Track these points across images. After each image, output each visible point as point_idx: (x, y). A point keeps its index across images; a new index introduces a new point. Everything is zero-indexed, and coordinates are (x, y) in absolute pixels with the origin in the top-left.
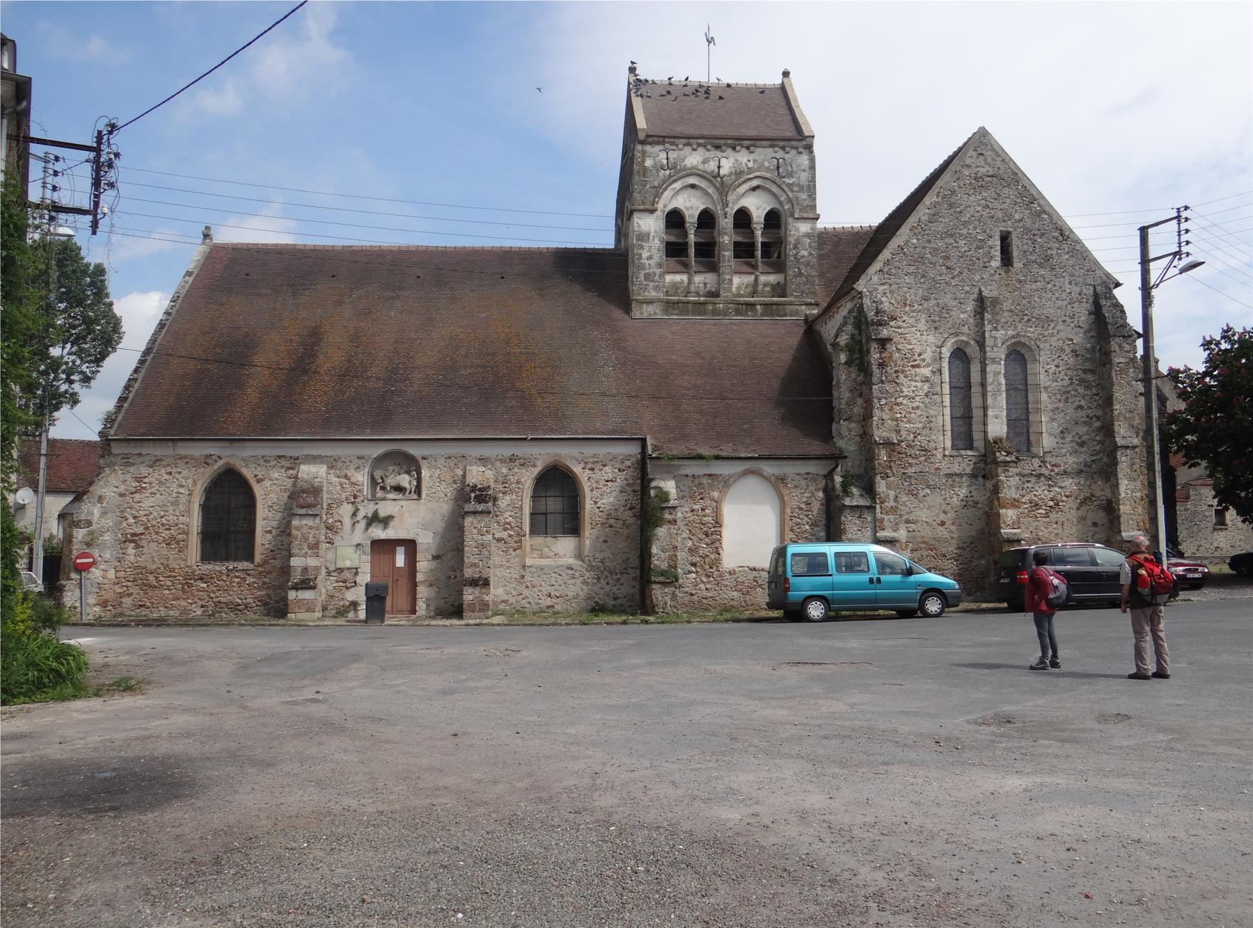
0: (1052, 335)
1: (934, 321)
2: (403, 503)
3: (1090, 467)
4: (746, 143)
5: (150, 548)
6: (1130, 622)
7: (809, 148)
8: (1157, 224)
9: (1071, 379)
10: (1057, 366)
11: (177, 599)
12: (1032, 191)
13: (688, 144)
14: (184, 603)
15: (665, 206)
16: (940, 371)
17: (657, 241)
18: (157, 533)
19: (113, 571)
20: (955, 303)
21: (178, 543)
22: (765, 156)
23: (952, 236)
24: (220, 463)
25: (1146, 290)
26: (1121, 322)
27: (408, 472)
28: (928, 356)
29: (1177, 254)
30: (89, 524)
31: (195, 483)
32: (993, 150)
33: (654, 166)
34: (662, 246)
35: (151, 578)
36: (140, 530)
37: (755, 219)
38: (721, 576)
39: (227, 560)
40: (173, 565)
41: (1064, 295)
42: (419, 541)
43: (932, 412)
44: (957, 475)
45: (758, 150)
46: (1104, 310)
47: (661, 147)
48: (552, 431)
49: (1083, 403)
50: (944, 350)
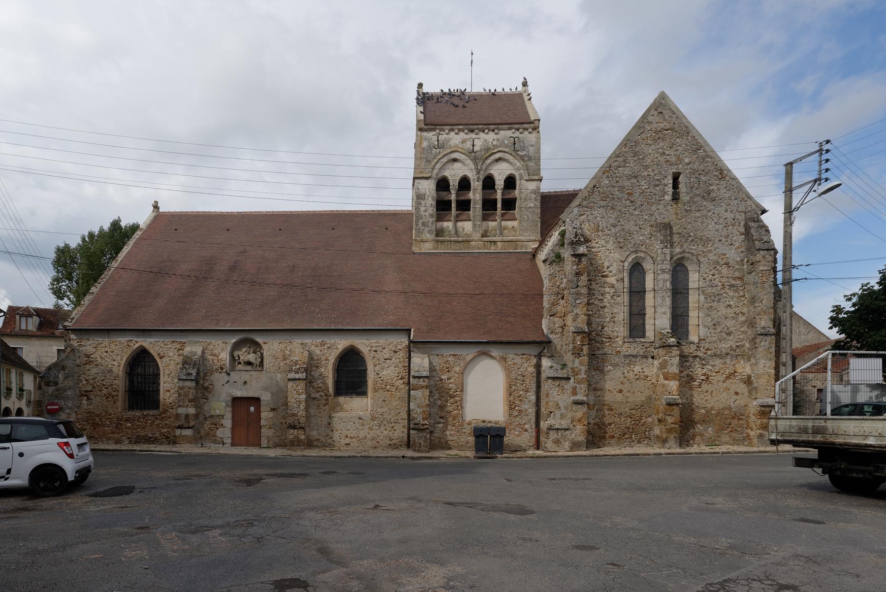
0: (710, 251)
1: (619, 242)
2: (252, 373)
3: (735, 351)
4: (492, 127)
5: (96, 401)
6: (348, 399)
7: (536, 128)
8: (800, 159)
9: (723, 285)
10: (713, 275)
11: (112, 433)
12: (700, 140)
13: (452, 130)
14: (118, 436)
15: (437, 175)
16: (623, 279)
17: (430, 198)
18: (100, 391)
19: (74, 415)
20: (637, 228)
21: (113, 397)
22: (506, 134)
23: (635, 177)
24: (137, 345)
25: (789, 211)
26: (765, 239)
27: (255, 352)
28: (614, 269)
29: (817, 181)
30: (56, 384)
31: (122, 359)
32: (670, 109)
33: (429, 147)
34: (434, 203)
35: (97, 419)
36: (89, 388)
37: (497, 182)
38: (462, 425)
39: (145, 409)
40: (110, 411)
41: (721, 221)
42: (262, 399)
43: (615, 310)
44: (633, 356)
45: (502, 132)
46: (752, 231)
47: (434, 133)
48: (348, 324)
49: (732, 303)
50: (626, 264)
